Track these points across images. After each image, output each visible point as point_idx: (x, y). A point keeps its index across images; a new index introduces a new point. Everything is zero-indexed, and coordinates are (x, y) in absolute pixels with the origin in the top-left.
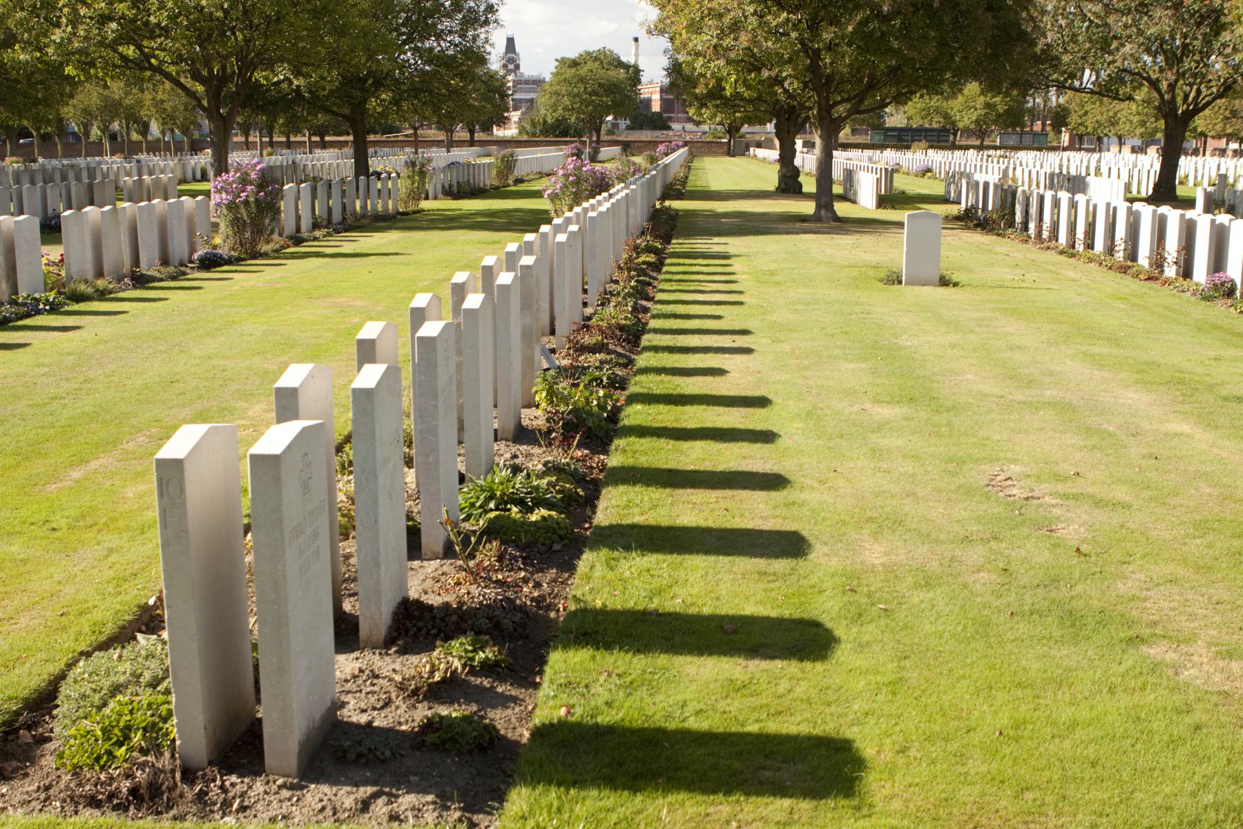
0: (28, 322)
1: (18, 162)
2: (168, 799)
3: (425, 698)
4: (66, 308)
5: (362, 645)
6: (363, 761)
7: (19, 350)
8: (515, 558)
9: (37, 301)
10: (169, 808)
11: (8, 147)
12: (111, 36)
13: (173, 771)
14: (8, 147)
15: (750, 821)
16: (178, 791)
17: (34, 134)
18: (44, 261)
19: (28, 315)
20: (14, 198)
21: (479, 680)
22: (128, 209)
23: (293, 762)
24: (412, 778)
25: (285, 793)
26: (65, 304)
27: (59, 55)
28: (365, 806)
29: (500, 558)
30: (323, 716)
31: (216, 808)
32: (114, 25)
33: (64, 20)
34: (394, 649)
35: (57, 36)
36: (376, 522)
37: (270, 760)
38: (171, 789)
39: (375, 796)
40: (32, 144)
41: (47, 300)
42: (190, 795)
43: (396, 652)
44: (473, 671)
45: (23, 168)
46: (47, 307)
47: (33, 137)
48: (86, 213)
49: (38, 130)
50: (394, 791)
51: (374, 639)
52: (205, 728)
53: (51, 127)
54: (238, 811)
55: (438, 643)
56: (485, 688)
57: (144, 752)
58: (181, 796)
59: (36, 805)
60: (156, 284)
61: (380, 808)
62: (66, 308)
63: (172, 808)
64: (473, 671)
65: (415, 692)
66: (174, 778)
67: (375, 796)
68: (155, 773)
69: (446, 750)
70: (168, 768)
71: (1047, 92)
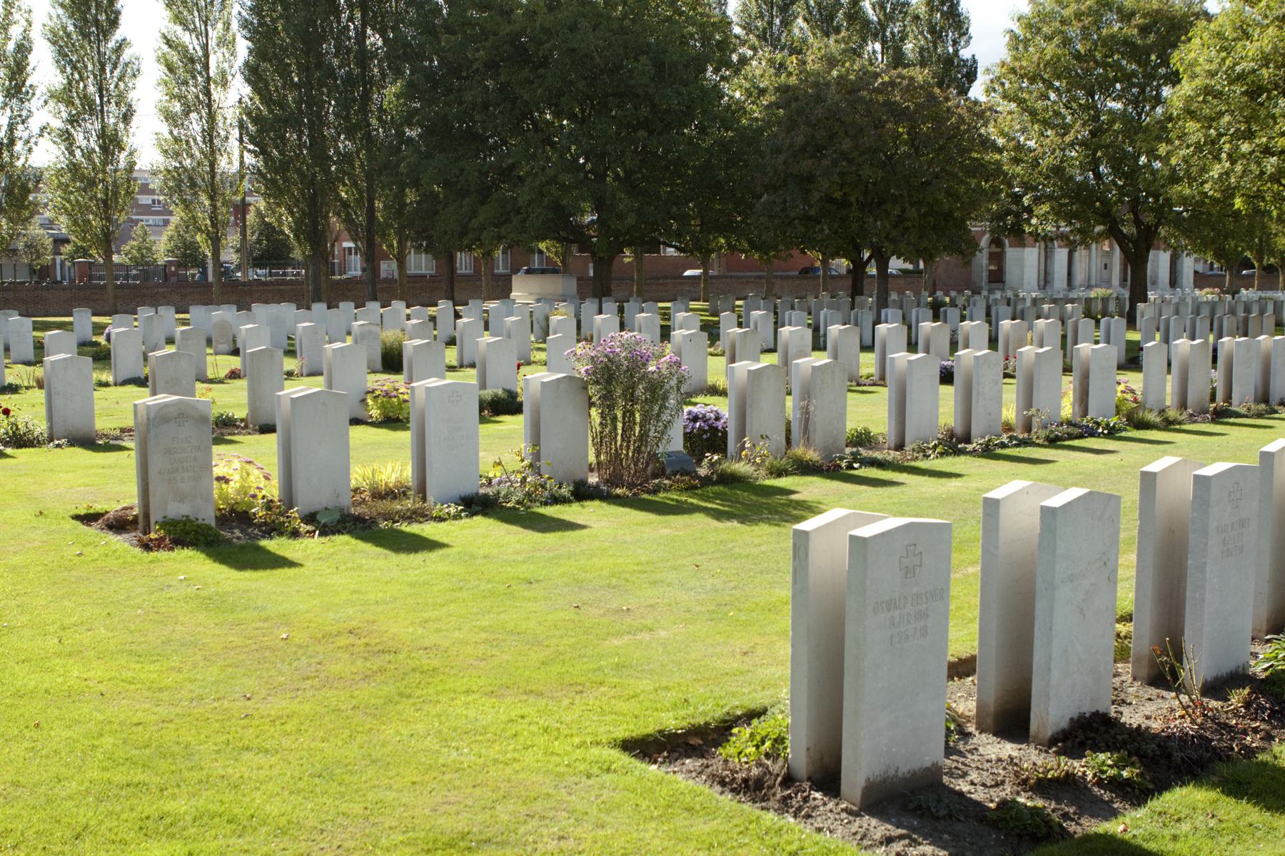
0: (1076, 443)
1: (1213, 293)
2: (765, 794)
3: (1032, 789)
4: (1123, 434)
5: (1031, 739)
6: (919, 812)
7: (1040, 466)
8: (1263, 709)
9: (1098, 424)
10: (763, 800)
11: (1281, 279)
12: (1270, 170)
13: (778, 775)
14: (1228, 278)
15: (334, 633)
16: (773, 791)
17: (1256, 264)
18: (1121, 387)
19: (1081, 437)
20: (1162, 328)
21: (1103, 792)
22: (1226, 345)
23: (857, 794)
24: (946, 836)
25: (844, 815)
26: (1125, 430)
27: (1215, 191)
28: (889, 840)
29: (1247, 705)
30: (914, 773)
31: (791, 810)
32: (1274, 160)
33: (1224, 156)
34: (1054, 749)
35: (1216, 170)
36: (1051, 629)
37: (844, 788)
38: (770, 788)
39: (901, 837)
40: (1252, 275)
41: (1108, 425)
42: (778, 796)
43: (1054, 752)
44: (1100, 783)
45: (1217, 299)
46: (1106, 432)
47: (1254, 268)
48: (1176, 345)
49: (1260, 260)
50: (920, 840)
51: (1041, 736)
52: (808, 749)
53: (1275, 258)
54: (803, 817)
55: (1088, 752)
56: (1103, 801)
57: (767, 756)
58: (774, 795)
59: (694, 774)
60: (1232, 420)
61: (897, 847)
62: (1123, 434)
63: (764, 801)
64: (1100, 783)
65: (1025, 782)
66: (775, 780)
67: (901, 837)
68: (765, 774)
69: (997, 828)
70: (775, 772)
71: (1196, 252)
